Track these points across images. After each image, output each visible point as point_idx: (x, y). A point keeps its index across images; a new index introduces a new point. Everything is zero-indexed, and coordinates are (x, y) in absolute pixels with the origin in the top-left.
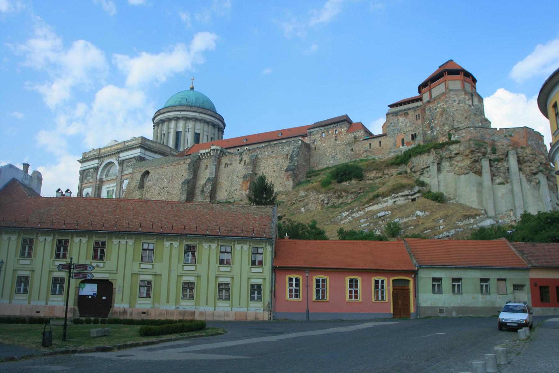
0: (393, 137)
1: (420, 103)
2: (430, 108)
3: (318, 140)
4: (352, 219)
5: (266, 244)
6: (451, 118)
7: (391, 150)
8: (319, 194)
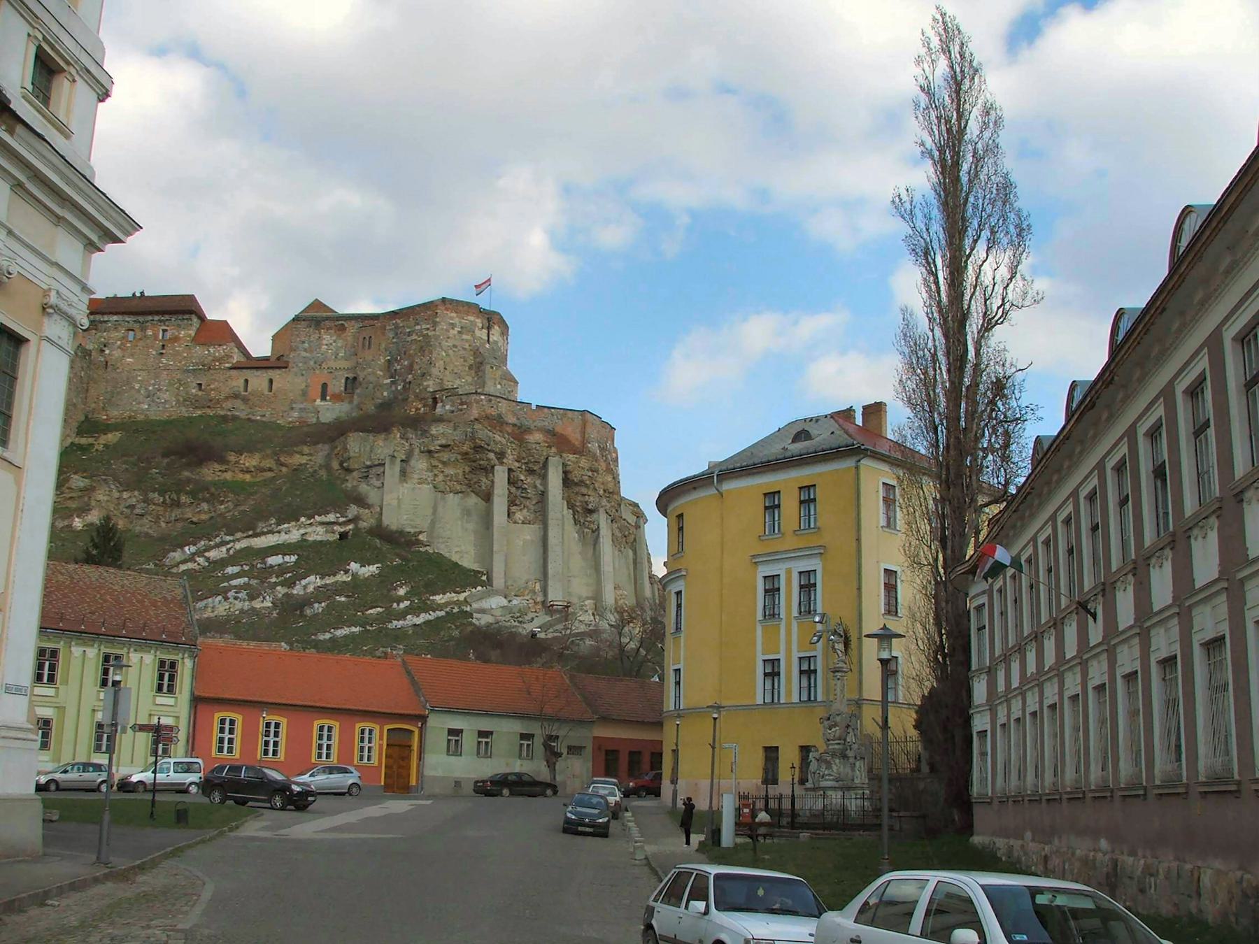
0: (303, 375)
2: (397, 327)
4: (207, 564)
5: (183, 655)
6: (442, 362)
7: (294, 406)
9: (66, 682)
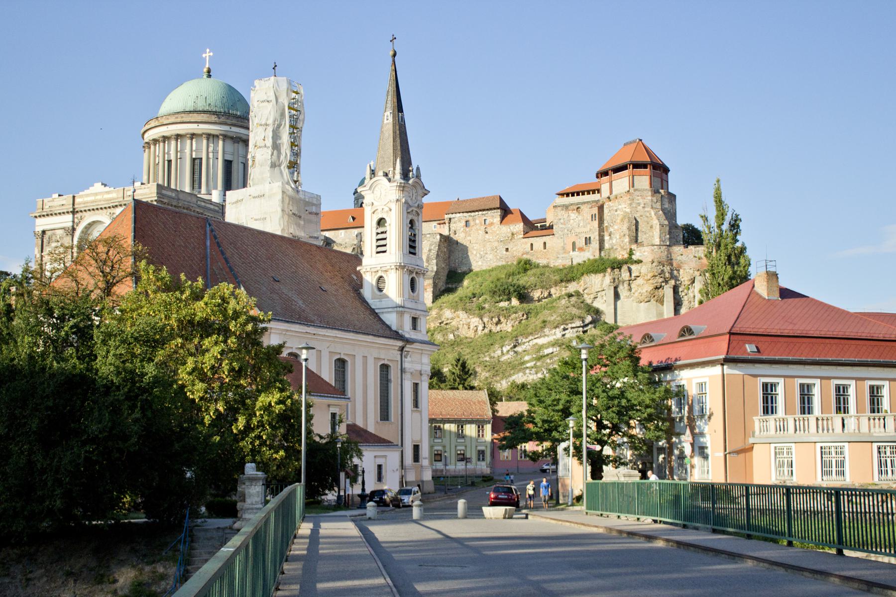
1: (596, 197)
2: (610, 207)
3: (461, 231)
8: (471, 317)
9: (445, 437)
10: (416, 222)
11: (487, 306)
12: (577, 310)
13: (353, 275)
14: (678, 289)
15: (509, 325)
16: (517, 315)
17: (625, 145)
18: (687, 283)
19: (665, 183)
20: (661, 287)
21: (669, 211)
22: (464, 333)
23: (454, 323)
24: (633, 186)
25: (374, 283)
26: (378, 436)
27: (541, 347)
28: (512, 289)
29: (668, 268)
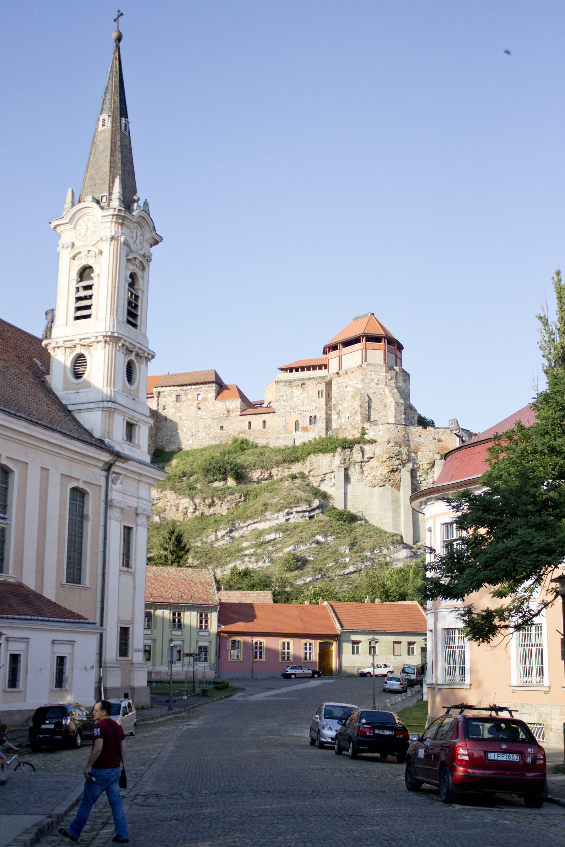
1: (323, 372)
7: (279, 436)
8: (180, 497)
9: (155, 627)
10: (140, 279)
11: (198, 486)
12: (303, 493)
13: (35, 359)
14: (416, 473)
15: (225, 507)
16: (233, 497)
17: (355, 319)
18: (426, 467)
19: (398, 360)
20: (397, 470)
21: (404, 391)
22: (171, 515)
23: (160, 504)
24: (366, 361)
25: (69, 363)
26: (60, 607)
27: (261, 533)
28: (229, 467)
29: (406, 450)
